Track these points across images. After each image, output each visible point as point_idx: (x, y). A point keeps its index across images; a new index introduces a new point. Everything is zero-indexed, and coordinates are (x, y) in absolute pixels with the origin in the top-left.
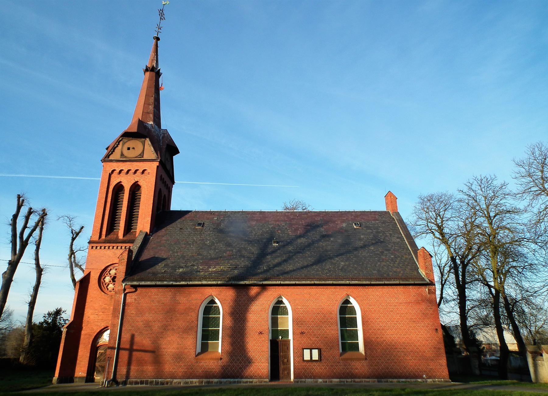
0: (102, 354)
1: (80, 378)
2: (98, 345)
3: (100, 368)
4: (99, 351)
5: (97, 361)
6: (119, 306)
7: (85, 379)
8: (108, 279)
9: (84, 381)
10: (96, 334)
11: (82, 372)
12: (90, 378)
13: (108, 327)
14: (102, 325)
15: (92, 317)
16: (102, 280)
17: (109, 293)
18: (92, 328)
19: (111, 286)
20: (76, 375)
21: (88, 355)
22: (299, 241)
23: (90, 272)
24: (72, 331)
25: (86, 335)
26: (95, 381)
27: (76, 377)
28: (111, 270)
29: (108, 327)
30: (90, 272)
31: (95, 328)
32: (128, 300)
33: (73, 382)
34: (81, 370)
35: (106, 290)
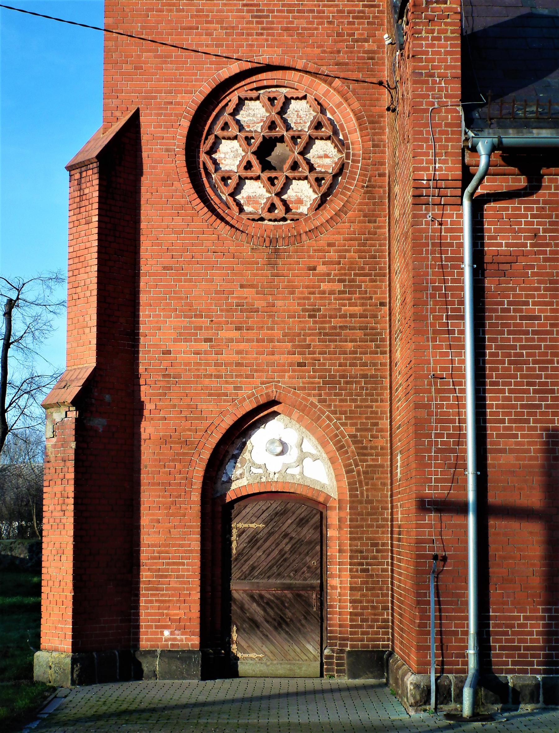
0: (254, 540)
1: (170, 654)
2: (230, 496)
3: (255, 609)
4: (237, 525)
5: (235, 573)
6: (449, 267)
7: (198, 658)
8: (231, 155)
9: (197, 670)
10: (217, 436)
11: (179, 625)
12: (216, 660)
13: (274, 403)
14: (244, 393)
15: (183, 352)
16: (203, 157)
17: (253, 227)
18: (193, 408)
19: (255, 192)
20: (145, 643)
21: (196, 545)
22: (75, 676)
23: (135, 117)
24: (99, 423)
25: (165, 441)
26: (242, 668)
27: (151, 653)
28: (241, 102)
29: (274, 403)
30: (135, 117)
31: (208, 407)
32: (498, 243)
33: (138, 675)
34: (168, 618)
35: (242, 222)
